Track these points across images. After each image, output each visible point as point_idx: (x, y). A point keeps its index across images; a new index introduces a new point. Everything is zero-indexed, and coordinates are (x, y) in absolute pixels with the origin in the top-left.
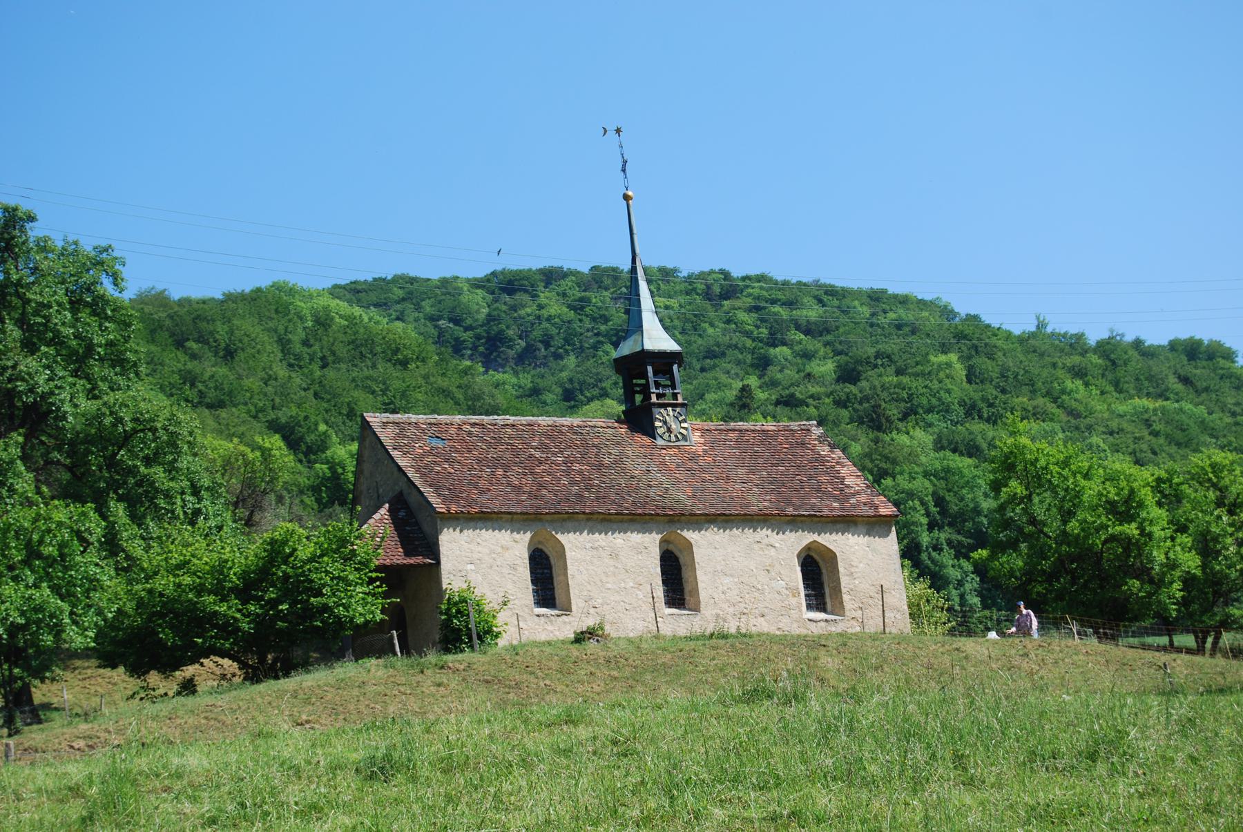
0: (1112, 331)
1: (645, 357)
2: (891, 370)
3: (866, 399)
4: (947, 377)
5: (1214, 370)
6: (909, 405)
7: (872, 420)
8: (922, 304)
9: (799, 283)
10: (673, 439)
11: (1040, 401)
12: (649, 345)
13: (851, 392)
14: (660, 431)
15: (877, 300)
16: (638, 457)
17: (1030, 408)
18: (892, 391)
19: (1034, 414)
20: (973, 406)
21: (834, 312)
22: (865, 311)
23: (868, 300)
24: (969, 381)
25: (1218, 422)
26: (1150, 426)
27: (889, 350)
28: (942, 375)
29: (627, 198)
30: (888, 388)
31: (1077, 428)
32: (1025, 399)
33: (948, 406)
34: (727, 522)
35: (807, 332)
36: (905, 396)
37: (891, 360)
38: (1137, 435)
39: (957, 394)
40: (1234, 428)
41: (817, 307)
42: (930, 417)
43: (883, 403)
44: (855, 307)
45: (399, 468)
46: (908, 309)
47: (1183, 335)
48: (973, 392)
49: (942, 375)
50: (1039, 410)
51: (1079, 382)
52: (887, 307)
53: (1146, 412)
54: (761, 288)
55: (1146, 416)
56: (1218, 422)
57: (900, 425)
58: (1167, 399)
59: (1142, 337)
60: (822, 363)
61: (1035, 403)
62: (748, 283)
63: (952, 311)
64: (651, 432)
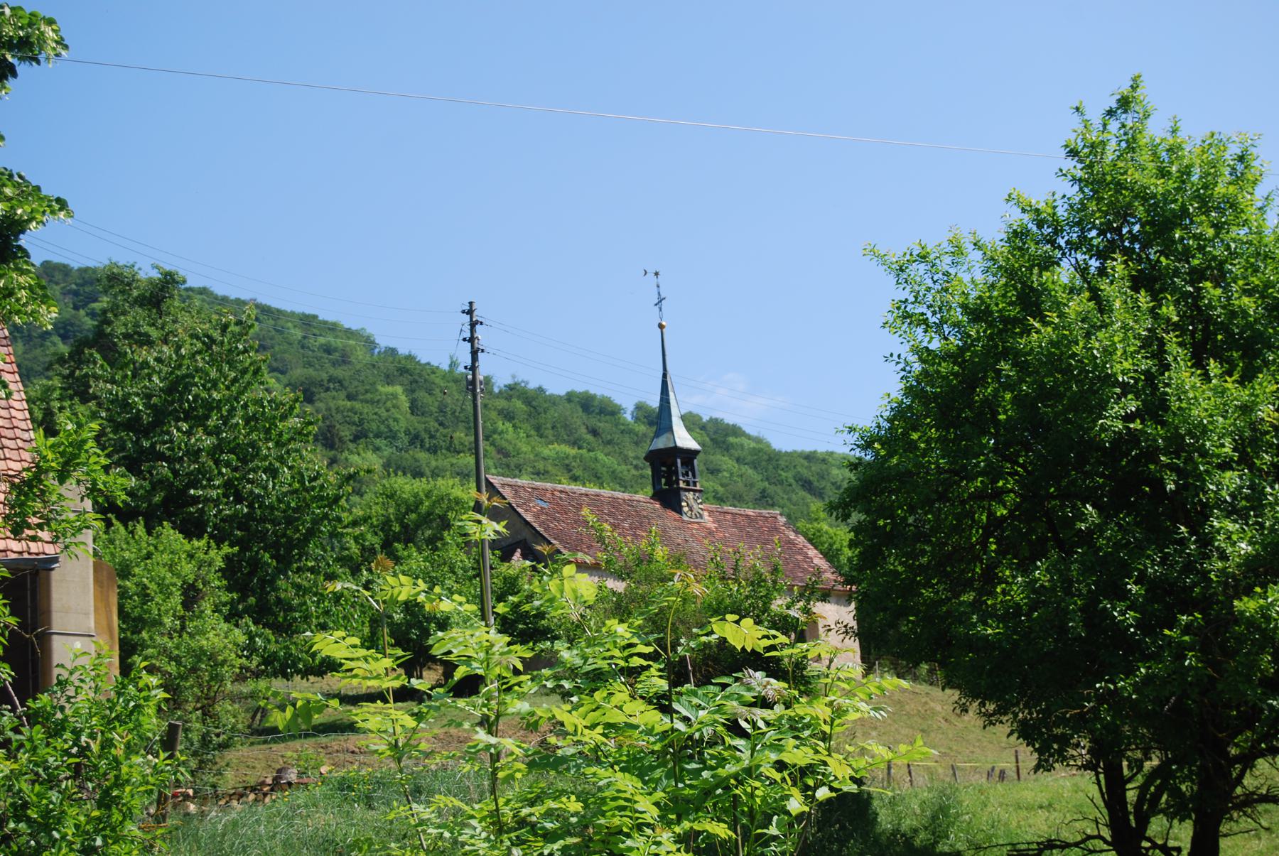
1: (676, 451)
2: (342, 394)
4: (394, 407)
5: (616, 425)
7: (326, 439)
8: (350, 333)
12: (680, 443)
14: (686, 509)
17: (467, 443)
18: (345, 414)
20: (417, 437)
22: (297, 334)
24: (412, 413)
25: (626, 473)
26: (570, 471)
27: (341, 376)
28: (389, 404)
29: (661, 326)
31: (508, 466)
32: (462, 435)
33: (396, 434)
36: (357, 420)
37: (342, 385)
39: (403, 424)
40: (640, 481)
42: (378, 442)
45: (527, 523)
47: (580, 388)
48: (417, 424)
49: (389, 404)
51: (509, 425)
52: (317, 332)
53: (567, 458)
55: (567, 462)
56: (626, 473)
57: (351, 446)
58: (580, 448)
63: (373, 342)
64: (680, 511)
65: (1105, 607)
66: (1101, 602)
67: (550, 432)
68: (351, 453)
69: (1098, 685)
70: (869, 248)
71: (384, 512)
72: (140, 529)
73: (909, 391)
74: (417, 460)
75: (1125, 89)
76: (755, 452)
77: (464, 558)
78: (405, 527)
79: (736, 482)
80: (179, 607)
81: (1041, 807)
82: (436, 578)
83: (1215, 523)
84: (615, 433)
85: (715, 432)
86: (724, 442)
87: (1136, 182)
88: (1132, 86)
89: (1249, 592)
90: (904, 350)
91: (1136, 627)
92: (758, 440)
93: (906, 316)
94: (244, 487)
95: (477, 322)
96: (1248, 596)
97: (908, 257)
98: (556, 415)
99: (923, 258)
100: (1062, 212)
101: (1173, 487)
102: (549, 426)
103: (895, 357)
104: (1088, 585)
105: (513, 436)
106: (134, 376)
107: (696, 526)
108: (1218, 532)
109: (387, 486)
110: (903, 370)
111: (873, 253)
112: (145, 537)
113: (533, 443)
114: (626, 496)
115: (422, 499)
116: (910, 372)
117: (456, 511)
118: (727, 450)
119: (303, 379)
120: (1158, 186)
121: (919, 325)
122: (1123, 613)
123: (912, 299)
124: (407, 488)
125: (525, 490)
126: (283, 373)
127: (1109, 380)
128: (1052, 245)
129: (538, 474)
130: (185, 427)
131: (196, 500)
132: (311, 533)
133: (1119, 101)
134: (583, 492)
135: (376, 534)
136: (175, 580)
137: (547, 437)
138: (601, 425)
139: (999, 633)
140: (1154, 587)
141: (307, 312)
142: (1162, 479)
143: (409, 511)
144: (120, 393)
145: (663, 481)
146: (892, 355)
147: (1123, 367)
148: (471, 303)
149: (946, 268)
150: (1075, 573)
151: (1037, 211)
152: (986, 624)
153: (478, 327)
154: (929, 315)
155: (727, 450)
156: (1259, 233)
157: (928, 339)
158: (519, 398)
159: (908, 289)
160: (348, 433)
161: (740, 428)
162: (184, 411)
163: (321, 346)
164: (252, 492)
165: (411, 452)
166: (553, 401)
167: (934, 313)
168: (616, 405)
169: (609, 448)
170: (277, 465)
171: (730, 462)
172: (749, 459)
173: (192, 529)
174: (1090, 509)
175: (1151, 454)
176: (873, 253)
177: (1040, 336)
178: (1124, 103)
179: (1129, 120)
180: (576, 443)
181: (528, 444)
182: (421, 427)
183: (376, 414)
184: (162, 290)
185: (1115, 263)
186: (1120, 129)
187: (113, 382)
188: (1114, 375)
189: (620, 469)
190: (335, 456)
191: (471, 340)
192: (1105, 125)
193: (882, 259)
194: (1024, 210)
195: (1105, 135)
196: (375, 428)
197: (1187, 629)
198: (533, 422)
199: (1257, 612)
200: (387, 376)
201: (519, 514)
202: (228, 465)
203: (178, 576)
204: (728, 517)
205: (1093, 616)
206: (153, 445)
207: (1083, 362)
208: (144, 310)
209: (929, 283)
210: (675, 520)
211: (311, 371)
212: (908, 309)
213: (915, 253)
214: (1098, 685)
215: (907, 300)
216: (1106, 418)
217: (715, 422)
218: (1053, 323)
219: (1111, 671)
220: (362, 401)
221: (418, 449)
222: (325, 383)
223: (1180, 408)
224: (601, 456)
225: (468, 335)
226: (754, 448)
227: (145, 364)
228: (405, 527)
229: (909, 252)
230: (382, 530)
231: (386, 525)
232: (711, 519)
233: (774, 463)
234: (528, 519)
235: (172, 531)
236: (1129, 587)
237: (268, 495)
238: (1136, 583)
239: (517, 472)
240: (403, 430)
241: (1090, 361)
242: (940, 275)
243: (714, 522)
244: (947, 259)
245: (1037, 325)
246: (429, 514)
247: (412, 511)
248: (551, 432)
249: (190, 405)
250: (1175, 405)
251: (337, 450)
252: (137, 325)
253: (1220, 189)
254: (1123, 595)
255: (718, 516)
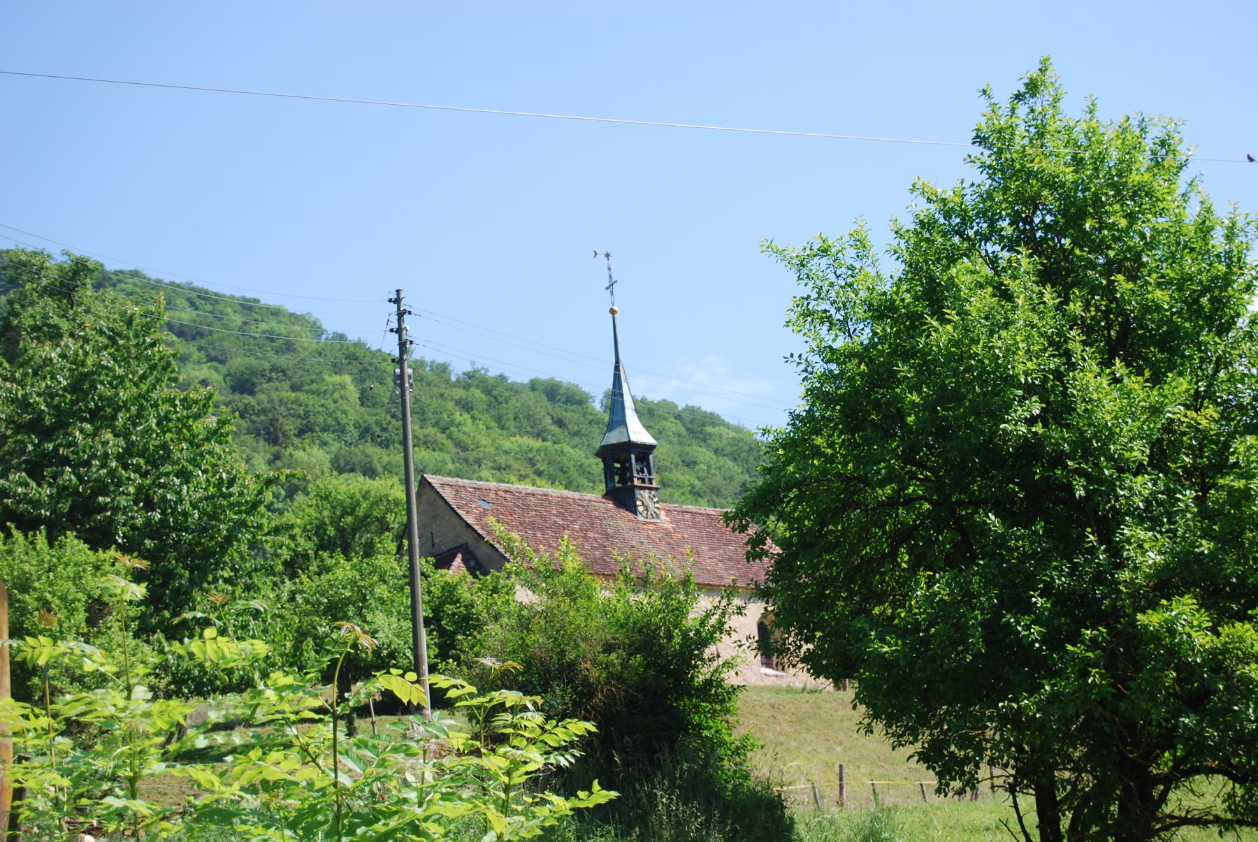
0: (473, 363)
2: (287, 385)
3: (264, 411)
4: (342, 397)
5: (584, 415)
6: (305, 422)
7: (268, 433)
9: (172, 284)
10: (650, 516)
11: (431, 431)
13: (249, 403)
14: (641, 509)
15: (250, 309)
16: (630, 530)
17: (421, 437)
18: (289, 406)
19: (425, 443)
21: (207, 317)
22: (238, 319)
23: (240, 308)
24: (362, 405)
26: (534, 465)
28: (336, 395)
29: (613, 312)
30: (286, 404)
31: (466, 461)
33: (344, 427)
34: (710, 590)
35: (180, 334)
36: (302, 412)
37: (285, 375)
38: (523, 473)
39: (352, 416)
41: (189, 310)
42: (326, 436)
43: (281, 418)
44: (227, 315)
45: (468, 525)
46: (280, 322)
47: (544, 375)
48: (369, 417)
49: (336, 395)
50: (429, 439)
51: (466, 416)
52: (259, 318)
54: (135, 285)
55: (530, 455)
57: (296, 440)
58: (544, 440)
59: (506, 374)
60: (197, 367)
61: (426, 431)
62: (121, 277)
64: (634, 510)
65: (1008, 622)
66: (1004, 616)
67: (511, 424)
68: (296, 448)
69: (1000, 705)
70: (767, 244)
71: (319, 516)
72: (41, 539)
73: (815, 395)
74: (367, 456)
75: (1034, 73)
76: (735, 442)
77: (395, 565)
78: (341, 531)
79: (714, 475)
80: (84, 624)
81: (987, 829)
82: (364, 587)
83: (1125, 531)
84: (583, 423)
85: (691, 422)
86: (700, 432)
87: (1043, 171)
88: (1041, 70)
89: (1153, 605)
90: (804, 349)
91: (1041, 643)
92: (738, 430)
93: (807, 314)
94: (155, 492)
95: (405, 312)
96: (1154, 609)
97: (808, 252)
98: (518, 405)
99: (825, 251)
100: (969, 201)
101: (1083, 493)
102: (511, 416)
103: (796, 357)
104: (990, 598)
105: (473, 429)
106: (35, 374)
107: (651, 527)
108: (1128, 541)
109: (321, 487)
110: (806, 370)
111: (770, 248)
112: (46, 548)
113: (493, 436)
114: (576, 495)
115: (358, 501)
116: (812, 373)
117: (396, 514)
118: (705, 440)
119: (243, 368)
120: (1068, 176)
121: (822, 323)
122: (1028, 628)
123: (814, 295)
124: (343, 488)
125: (466, 490)
126: (222, 362)
127: (1011, 381)
128: (961, 237)
129: (499, 469)
130: (88, 427)
131: (103, 508)
132: (229, 540)
133: (1026, 85)
134: (529, 491)
135: (310, 539)
136: (80, 595)
137: (508, 429)
138: (568, 415)
139: (897, 650)
140: (1060, 599)
141: (248, 296)
142: (1070, 485)
143: (345, 513)
144: (20, 394)
145: (617, 478)
146: (792, 355)
147: (1022, 367)
148: (398, 291)
149: (850, 261)
150: (976, 586)
151: (943, 200)
152: (883, 641)
153: (406, 317)
154: (833, 311)
155: (705, 440)
156: (1179, 222)
157: (833, 337)
158: (478, 387)
159: (811, 284)
160: (292, 427)
161: (718, 417)
162: (90, 411)
163: (263, 332)
164: (163, 498)
165: (361, 447)
166: (515, 389)
167: (838, 309)
168: (584, 393)
169: (577, 440)
170: (190, 467)
171: (708, 453)
172: (728, 450)
173: (99, 538)
174: (993, 518)
175: (1058, 459)
176: (770, 248)
177: (941, 335)
178: (1033, 87)
179: (1038, 103)
180: (540, 435)
181: (488, 436)
182: (371, 420)
183: (322, 405)
184: (72, 279)
185: (1019, 256)
186: (1029, 114)
187: (13, 380)
188: (1017, 376)
189: (588, 462)
190: (278, 452)
191: (399, 331)
192: (1013, 110)
193: (780, 253)
194: (929, 200)
195: (1013, 119)
196: (321, 421)
197: (1094, 644)
198: (494, 412)
199: (1161, 626)
200: (335, 365)
201: (460, 517)
202: (137, 469)
203: (84, 590)
204: (688, 516)
205: (995, 631)
206: (56, 449)
207: (983, 363)
208: (53, 301)
209: (832, 277)
210: (629, 521)
211: (252, 360)
212: (810, 307)
213: (816, 247)
214: (1000, 705)
215: (809, 297)
216: (1007, 422)
217: (691, 410)
218: (953, 321)
219: (1011, 689)
220: (307, 392)
221: (369, 444)
222: (267, 373)
223: (1086, 410)
224: (567, 449)
225: (395, 325)
226: (734, 438)
227: (48, 361)
228: (341, 531)
229: (809, 246)
230: (316, 534)
231: (320, 529)
232: (668, 519)
233: (755, 453)
234: (469, 522)
235: (76, 541)
236: (1034, 600)
237: (181, 501)
238: (1041, 596)
239: (476, 467)
240: (352, 423)
241: (991, 362)
242: (844, 270)
243: (671, 523)
244: (852, 252)
245: (935, 324)
246: (367, 516)
247: (349, 514)
248: (513, 423)
249: (96, 404)
250: (1081, 407)
251: (280, 445)
252: (45, 317)
253: (1135, 178)
254: (1028, 608)
255: (674, 514)
